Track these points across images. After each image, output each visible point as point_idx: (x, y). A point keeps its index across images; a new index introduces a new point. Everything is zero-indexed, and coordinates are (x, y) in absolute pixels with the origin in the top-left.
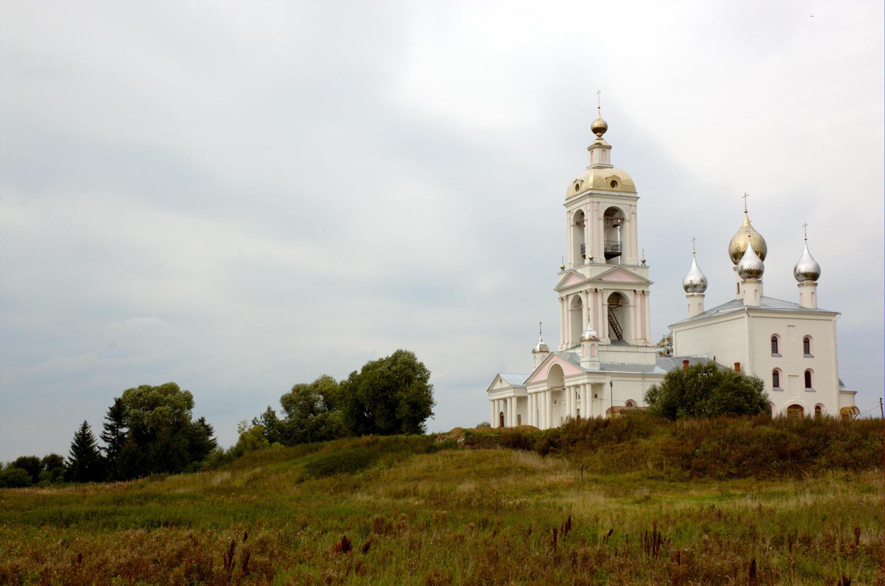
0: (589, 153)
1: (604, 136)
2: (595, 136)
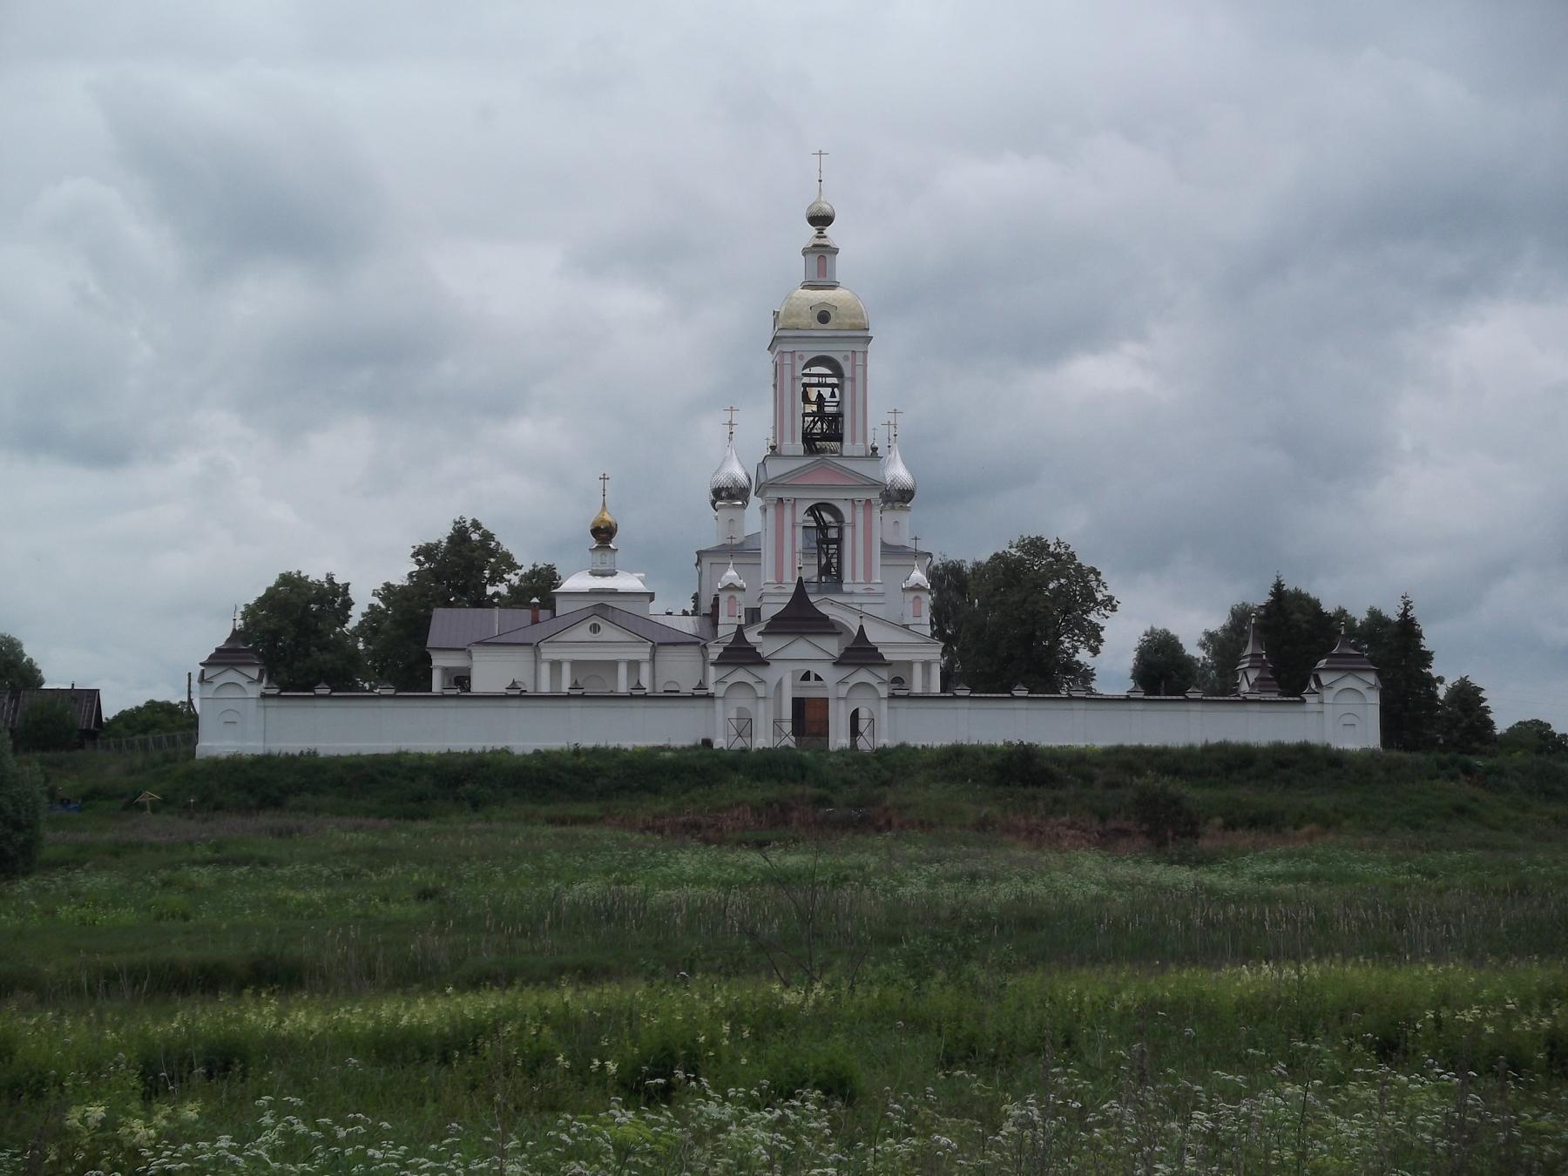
2: (813, 231)
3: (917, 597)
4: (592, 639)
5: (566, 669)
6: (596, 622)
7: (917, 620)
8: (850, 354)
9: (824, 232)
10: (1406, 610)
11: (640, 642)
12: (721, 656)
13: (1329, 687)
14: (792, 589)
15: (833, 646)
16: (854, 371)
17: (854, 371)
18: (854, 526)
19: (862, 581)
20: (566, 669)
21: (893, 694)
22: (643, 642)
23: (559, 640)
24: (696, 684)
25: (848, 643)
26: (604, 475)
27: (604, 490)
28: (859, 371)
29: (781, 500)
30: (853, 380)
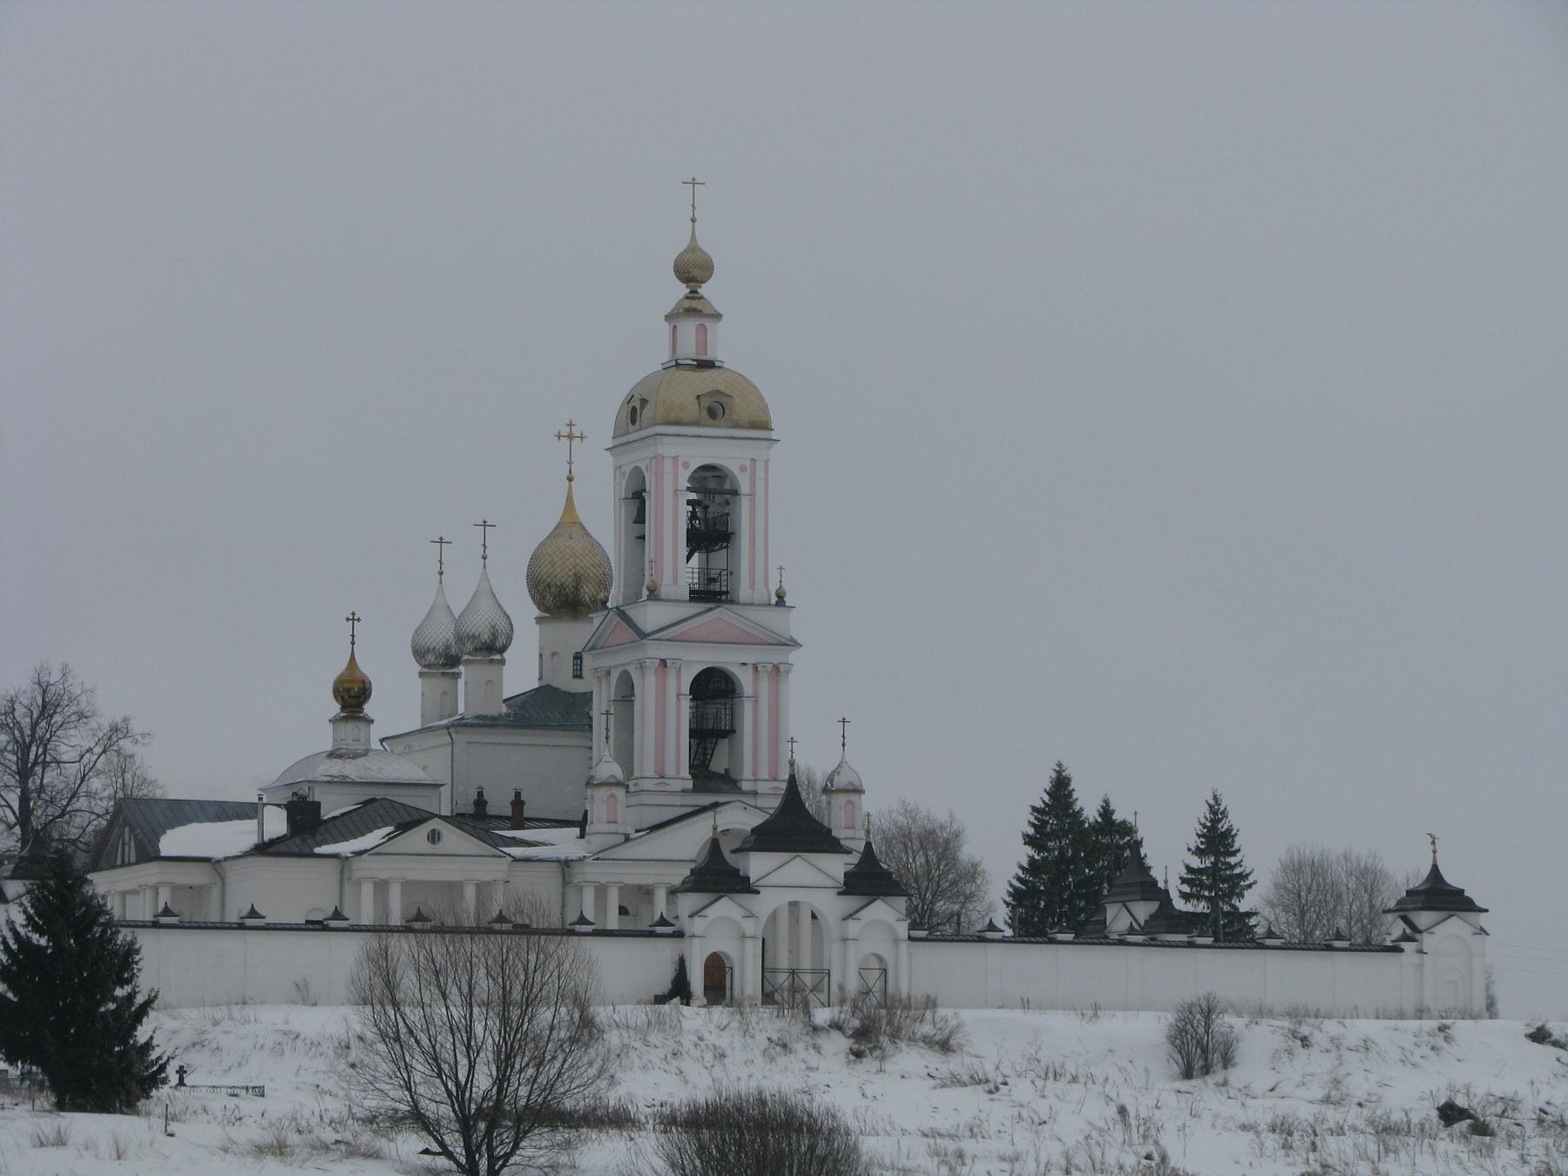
0: (567, 482)
1: (704, 290)
2: (683, 290)
3: (850, 802)
4: (431, 852)
5: (395, 892)
6: (433, 827)
7: (850, 833)
8: (748, 463)
9: (688, 291)
10: (1215, 822)
11: (494, 856)
12: (15, 870)
13: (1429, 929)
14: (784, 786)
15: (836, 866)
16: (753, 486)
17: (753, 486)
18: (756, 703)
19: (767, 777)
20: (395, 892)
21: (158, 922)
22: (500, 857)
23: (386, 851)
24: (330, 912)
25: (854, 859)
26: (353, 614)
27: (353, 636)
28: (760, 485)
29: (664, 662)
30: (752, 495)
